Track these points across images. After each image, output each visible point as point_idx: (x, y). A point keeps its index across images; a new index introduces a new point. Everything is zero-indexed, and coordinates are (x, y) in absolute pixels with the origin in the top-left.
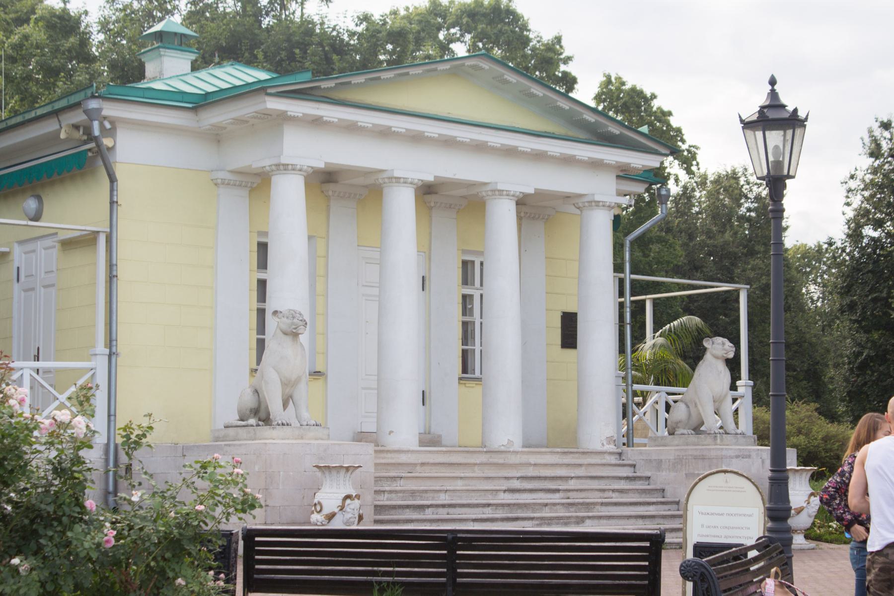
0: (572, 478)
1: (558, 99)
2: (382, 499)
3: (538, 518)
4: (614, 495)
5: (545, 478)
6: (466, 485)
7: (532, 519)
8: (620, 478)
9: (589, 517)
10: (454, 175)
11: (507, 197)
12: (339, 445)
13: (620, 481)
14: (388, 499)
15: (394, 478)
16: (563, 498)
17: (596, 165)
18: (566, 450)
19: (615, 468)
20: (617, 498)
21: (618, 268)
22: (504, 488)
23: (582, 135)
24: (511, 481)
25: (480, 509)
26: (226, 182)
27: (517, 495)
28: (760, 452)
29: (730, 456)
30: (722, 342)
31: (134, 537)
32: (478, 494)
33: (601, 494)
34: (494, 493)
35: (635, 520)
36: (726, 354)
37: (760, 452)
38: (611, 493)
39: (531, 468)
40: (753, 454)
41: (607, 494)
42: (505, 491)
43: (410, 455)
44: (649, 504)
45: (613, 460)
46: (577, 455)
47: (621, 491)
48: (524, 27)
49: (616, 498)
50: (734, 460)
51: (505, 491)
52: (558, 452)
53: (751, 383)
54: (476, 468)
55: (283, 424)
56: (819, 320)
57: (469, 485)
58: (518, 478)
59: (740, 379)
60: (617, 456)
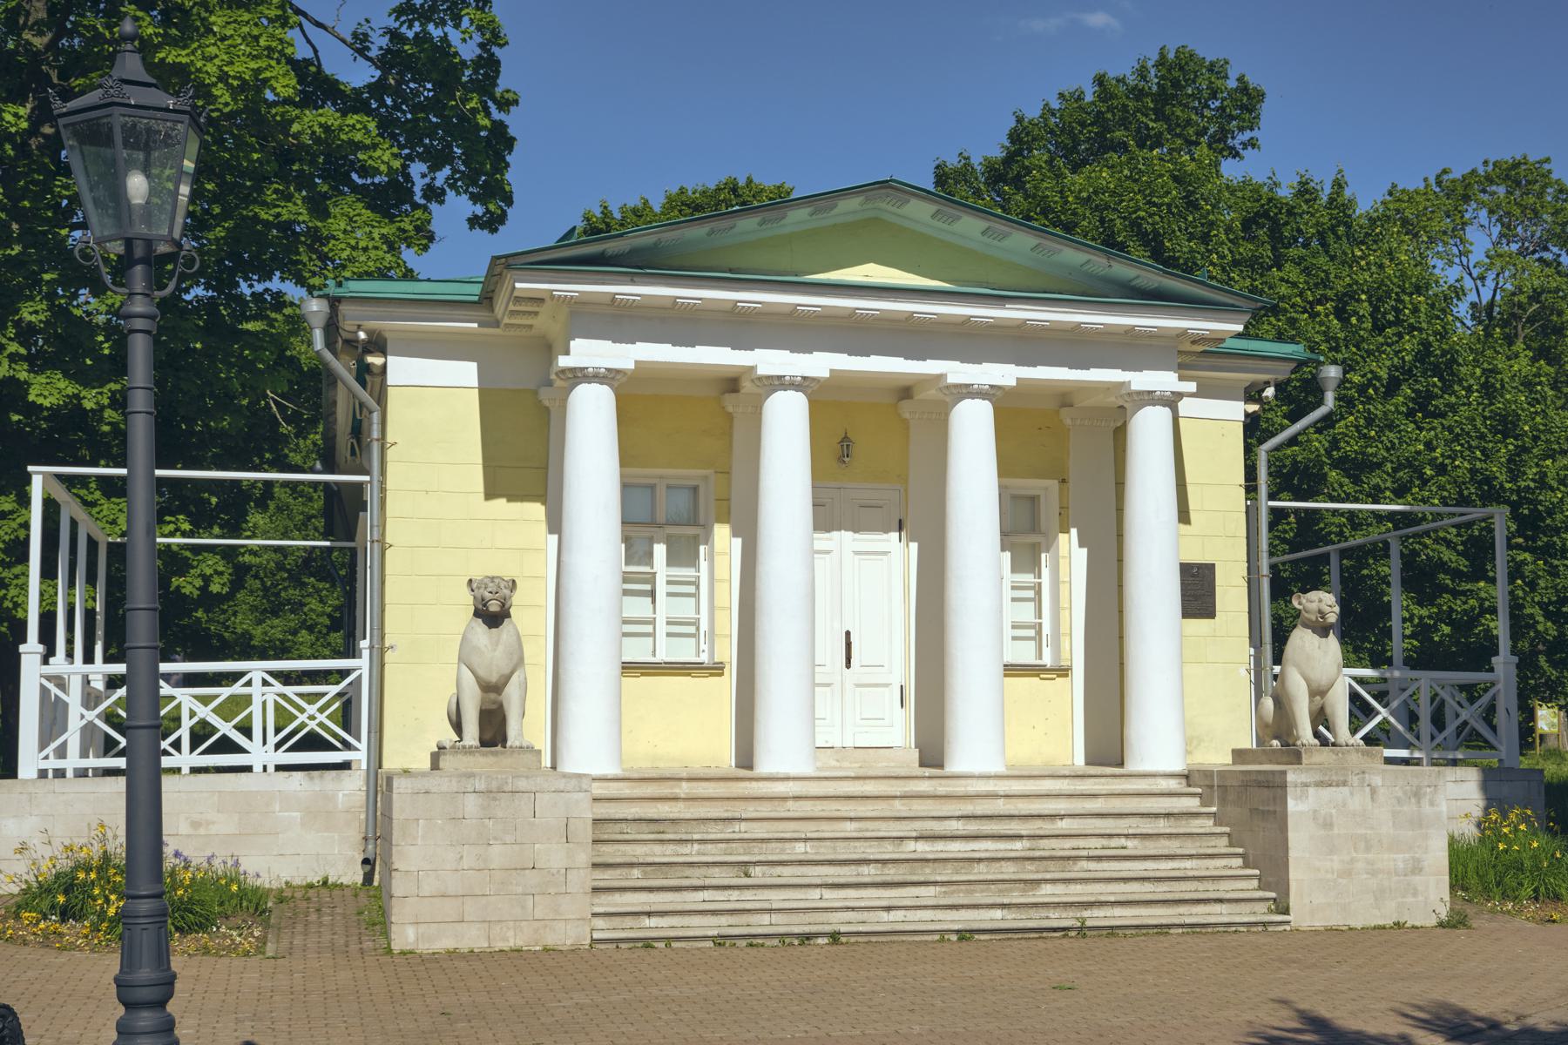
8: (1157, 816)
14: (699, 854)
21: (1251, 488)
34: (897, 842)
39: (1001, 802)
50: (1311, 790)
51: (916, 838)
60: (1184, 781)
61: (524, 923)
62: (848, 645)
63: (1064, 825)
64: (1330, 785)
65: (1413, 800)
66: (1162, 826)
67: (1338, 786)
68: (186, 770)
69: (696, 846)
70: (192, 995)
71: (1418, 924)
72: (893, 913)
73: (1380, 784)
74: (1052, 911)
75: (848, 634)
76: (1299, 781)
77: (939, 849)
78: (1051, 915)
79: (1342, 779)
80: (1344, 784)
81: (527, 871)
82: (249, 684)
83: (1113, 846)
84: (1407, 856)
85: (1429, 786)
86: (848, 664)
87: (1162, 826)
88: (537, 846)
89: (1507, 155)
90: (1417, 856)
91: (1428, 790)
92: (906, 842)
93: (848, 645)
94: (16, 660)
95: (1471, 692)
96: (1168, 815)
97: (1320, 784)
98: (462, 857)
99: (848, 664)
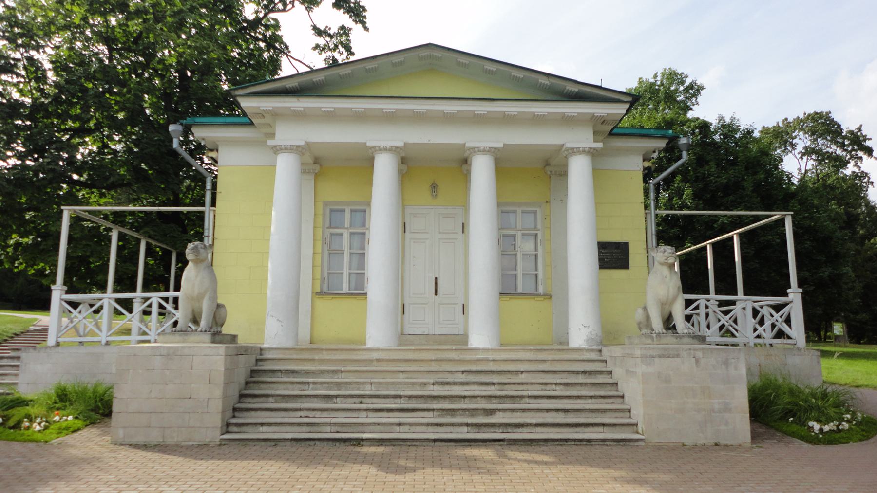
0: (522, 372)
1: (567, 84)
2: (307, 389)
3: (438, 410)
4: (558, 388)
5: (492, 372)
6: (408, 378)
7: (433, 410)
8: (578, 373)
9: (500, 410)
10: (430, 140)
11: (286, 151)
12: (189, 347)
13: (578, 375)
14: (312, 389)
15: (335, 372)
16: (499, 390)
17: (567, 121)
18: (417, 347)
19: (583, 363)
20: (561, 390)
21: (646, 207)
22: (432, 381)
23: (559, 98)
24: (456, 375)
25: (392, 399)
26: (307, 171)
27: (447, 387)
28: (692, 351)
29: (650, 356)
30: (664, 249)
31: (34, 425)
32: (406, 386)
33: (543, 387)
34: (423, 385)
35: (556, 413)
36: (666, 259)
37: (692, 351)
38: (554, 387)
39: (491, 364)
40: (684, 354)
41: (549, 387)
42: (433, 384)
43: (381, 353)
44: (586, 397)
45: (594, 356)
46: (553, 352)
47: (566, 385)
48: (839, 126)
49: (560, 391)
50: (656, 360)
51: (433, 384)
52: (531, 350)
53: (801, 290)
54: (433, 363)
55: (16, 335)
56: (75, 119)
57: (411, 378)
58: (463, 372)
59: (790, 287)
60: (598, 353)
61: (183, 429)
62: (436, 284)
63: (522, 378)
64: (669, 357)
65: (723, 367)
66: (581, 379)
67: (673, 357)
68: (741, 344)
69: (311, 386)
70: (365, 458)
71: (729, 443)
72: (402, 427)
73: (701, 356)
74: (498, 428)
75: (436, 279)
76: (649, 354)
77: (447, 389)
78: (497, 431)
79: (676, 353)
80: (678, 356)
81: (186, 400)
82: (697, 308)
83: (548, 389)
84: (720, 401)
85: (734, 358)
86: (436, 294)
87: (581, 379)
88: (193, 385)
89: (281, 24)
90: (727, 401)
91: (733, 360)
92: (428, 385)
93: (436, 284)
94: (49, 291)
95: (778, 308)
96: (584, 372)
97: (660, 356)
98: (151, 391)
99: (436, 294)
